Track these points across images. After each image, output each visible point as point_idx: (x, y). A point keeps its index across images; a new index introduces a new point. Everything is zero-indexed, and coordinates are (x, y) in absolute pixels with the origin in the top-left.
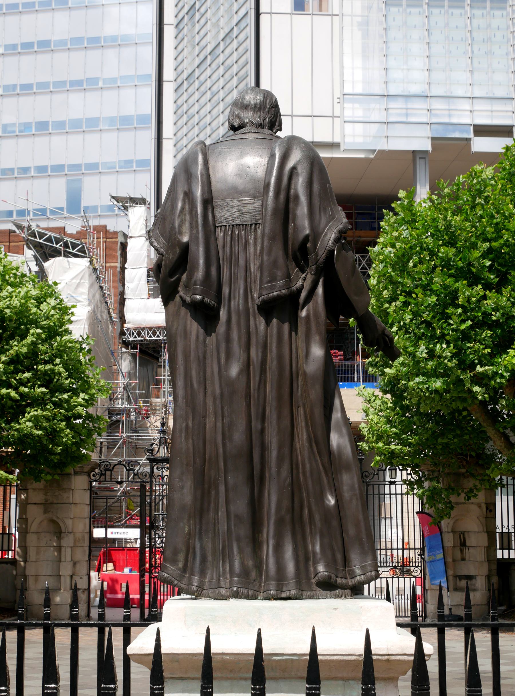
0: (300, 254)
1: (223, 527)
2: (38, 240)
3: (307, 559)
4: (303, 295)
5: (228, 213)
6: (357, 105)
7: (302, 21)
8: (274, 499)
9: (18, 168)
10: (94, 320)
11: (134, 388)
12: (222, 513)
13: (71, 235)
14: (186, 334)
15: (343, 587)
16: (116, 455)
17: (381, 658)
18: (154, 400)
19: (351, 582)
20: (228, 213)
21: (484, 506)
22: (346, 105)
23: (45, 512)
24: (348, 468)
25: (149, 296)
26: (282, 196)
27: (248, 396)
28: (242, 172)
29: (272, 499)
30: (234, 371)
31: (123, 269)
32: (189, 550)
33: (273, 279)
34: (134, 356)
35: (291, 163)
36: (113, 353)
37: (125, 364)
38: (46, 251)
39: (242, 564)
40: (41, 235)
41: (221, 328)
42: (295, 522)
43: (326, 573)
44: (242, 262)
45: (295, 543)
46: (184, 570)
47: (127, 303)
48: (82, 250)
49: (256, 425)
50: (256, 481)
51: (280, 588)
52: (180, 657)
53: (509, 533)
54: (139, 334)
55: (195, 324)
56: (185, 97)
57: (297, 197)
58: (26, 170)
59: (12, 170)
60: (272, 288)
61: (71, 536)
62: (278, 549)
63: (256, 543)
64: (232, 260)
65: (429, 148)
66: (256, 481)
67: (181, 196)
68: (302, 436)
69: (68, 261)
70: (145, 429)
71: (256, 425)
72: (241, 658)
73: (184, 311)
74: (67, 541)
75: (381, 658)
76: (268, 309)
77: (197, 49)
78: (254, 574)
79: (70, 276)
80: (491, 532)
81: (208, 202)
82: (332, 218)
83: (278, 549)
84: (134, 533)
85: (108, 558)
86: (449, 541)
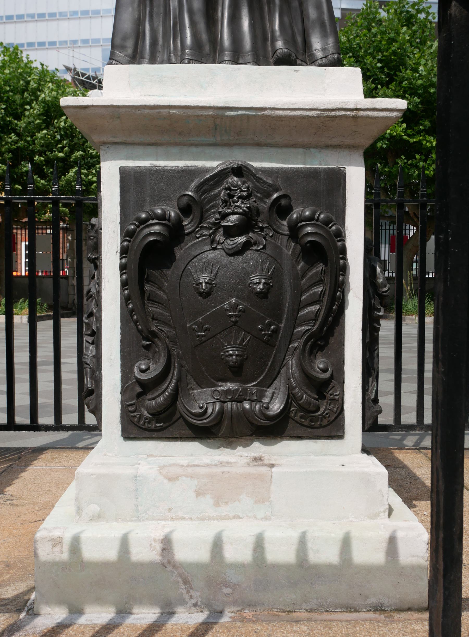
2: (81, 78)
9: (70, 41)
17: (347, 113)
40: (83, 75)
43: (286, 50)
52: (122, 110)
59: (66, 42)
69: (101, 93)
72: (190, 112)
75: (347, 113)
78: (207, 48)
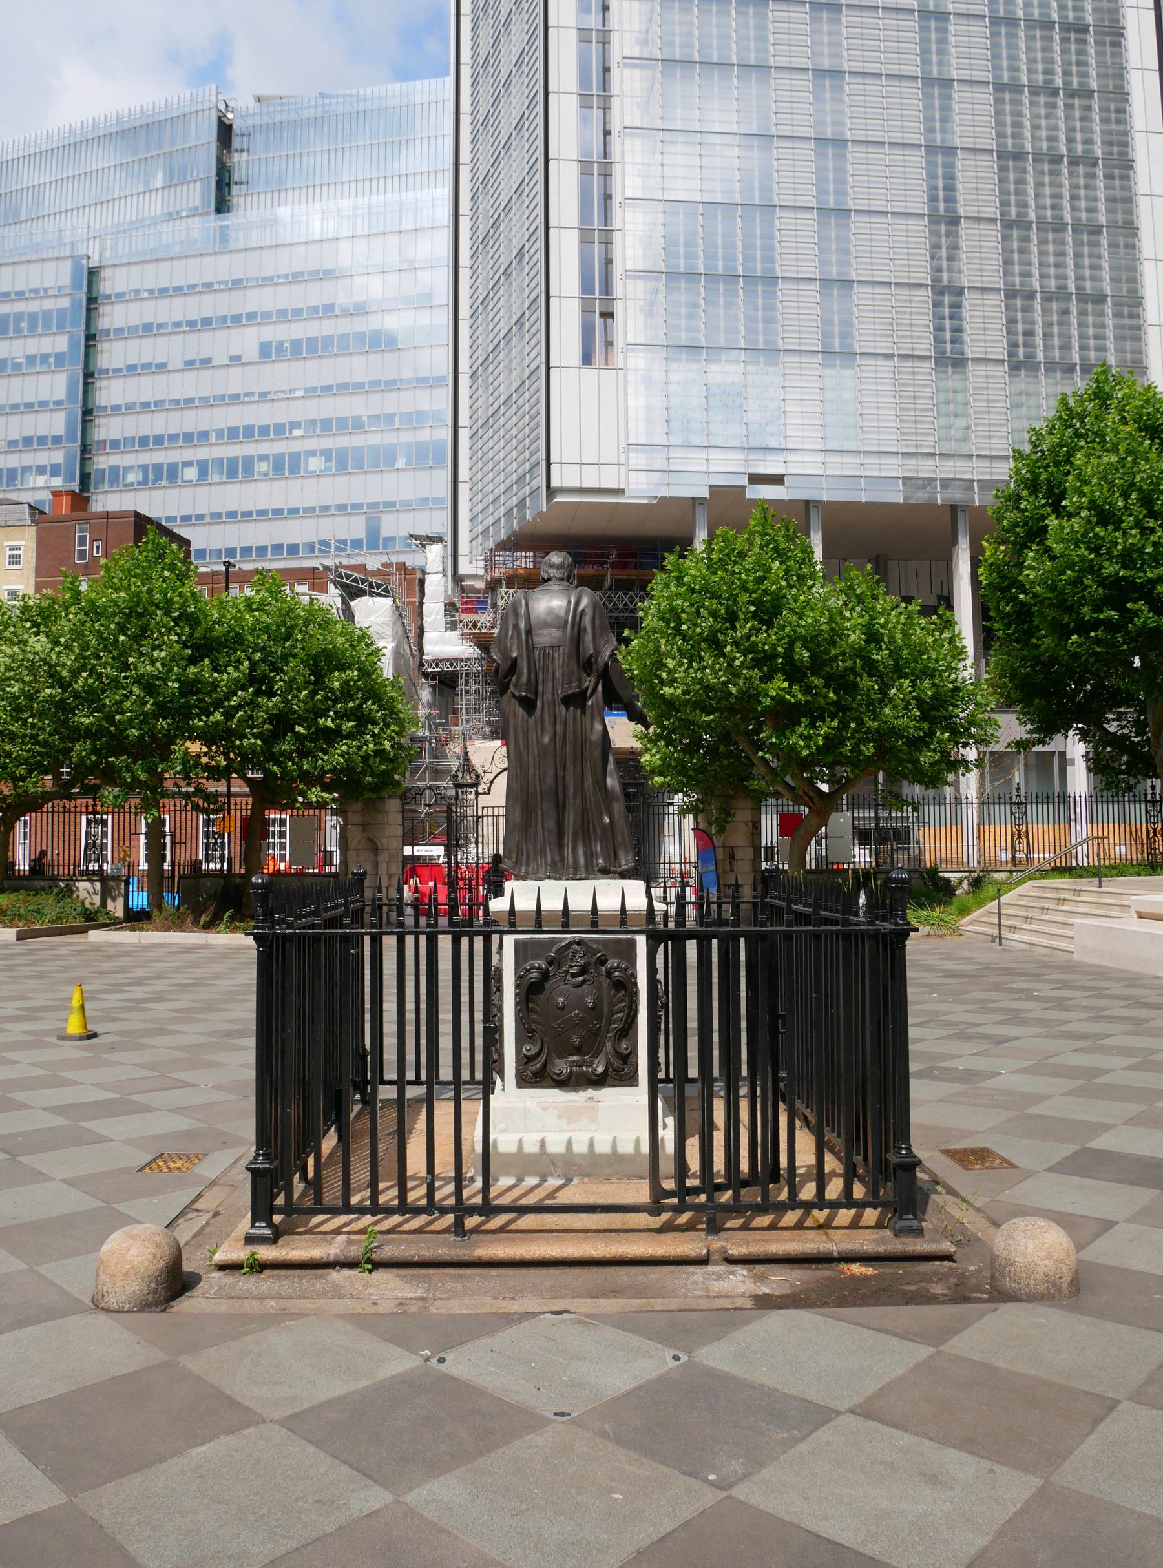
0: (587, 665)
1: (540, 836)
3: (592, 856)
4: (589, 691)
5: (545, 637)
6: (640, 455)
7: (589, 373)
8: (571, 819)
10: (398, 654)
11: (435, 718)
12: (539, 828)
13: (374, 574)
14: (515, 715)
15: (614, 873)
16: (419, 779)
18: (453, 728)
19: (619, 870)
20: (545, 637)
21: (750, 824)
22: (630, 455)
23: (363, 831)
24: (617, 800)
25: (447, 629)
26: (576, 629)
27: (555, 755)
28: (550, 611)
29: (570, 819)
30: (546, 739)
31: (421, 604)
32: (519, 851)
33: (570, 682)
34: (433, 687)
35: (581, 607)
36: (414, 685)
37: (425, 694)
38: (351, 592)
39: (552, 858)
41: (538, 712)
42: (585, 833)
44: (550, 670)
45: (584, 845)
46: (516, 863)
47: (426, 635)
48: (386, 590)
49: (560, 773)
50: (560, 808)
51: (575, 873)
53: (772, 848)
54: (437, 665)
55: (521, 710)
56: (480, 444)
57: (585, 629)
58: (326, 508)
59: (313, 509)
60: (570, 688)
61: (386, 853)
62: (574, 849)
63: (561, 847)
64: (544, 669)
65: (707, 495)
66: (560, 808)
67: (511, 627)
68: (589, 780)
70: (445, 756)
71: (560, 773)
73: (513, 700)
74: (383, 857)
76: (567, 701)
77: (491, 389)
79: (374, 614)
80: (756, 847)
81: (529, 632)
82: (607, 642)
83: (574, 849)
84: (439, 851)
85: (413, 872)
86: (720, 853)
